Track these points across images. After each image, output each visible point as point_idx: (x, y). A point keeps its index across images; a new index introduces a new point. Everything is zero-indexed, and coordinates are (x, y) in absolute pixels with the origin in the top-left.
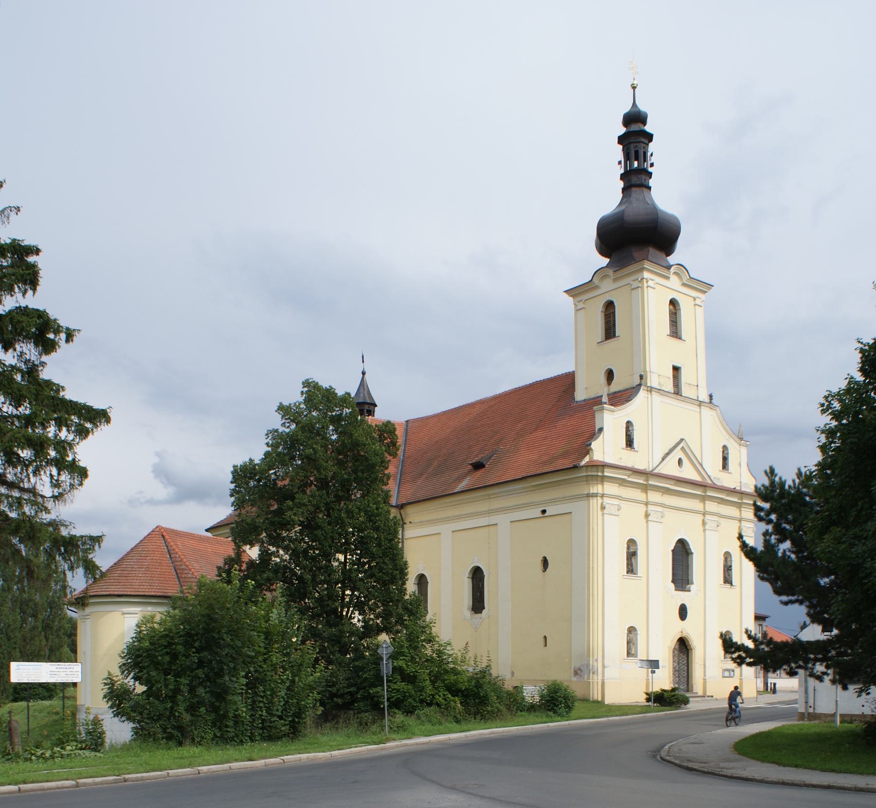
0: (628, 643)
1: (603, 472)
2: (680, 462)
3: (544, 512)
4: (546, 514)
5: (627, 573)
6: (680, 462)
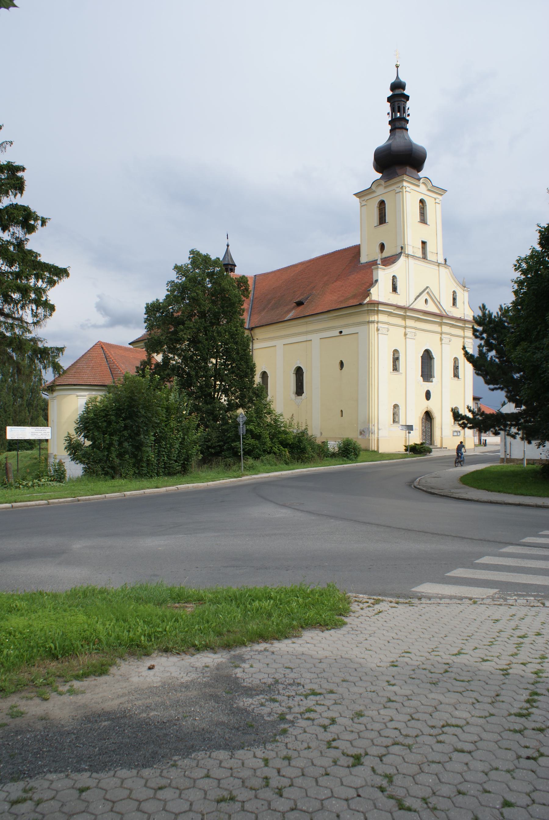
0: (394, 414)
1: (378, 307)
2: (426, 301)
3: (341, 332)
5: (393, 370)
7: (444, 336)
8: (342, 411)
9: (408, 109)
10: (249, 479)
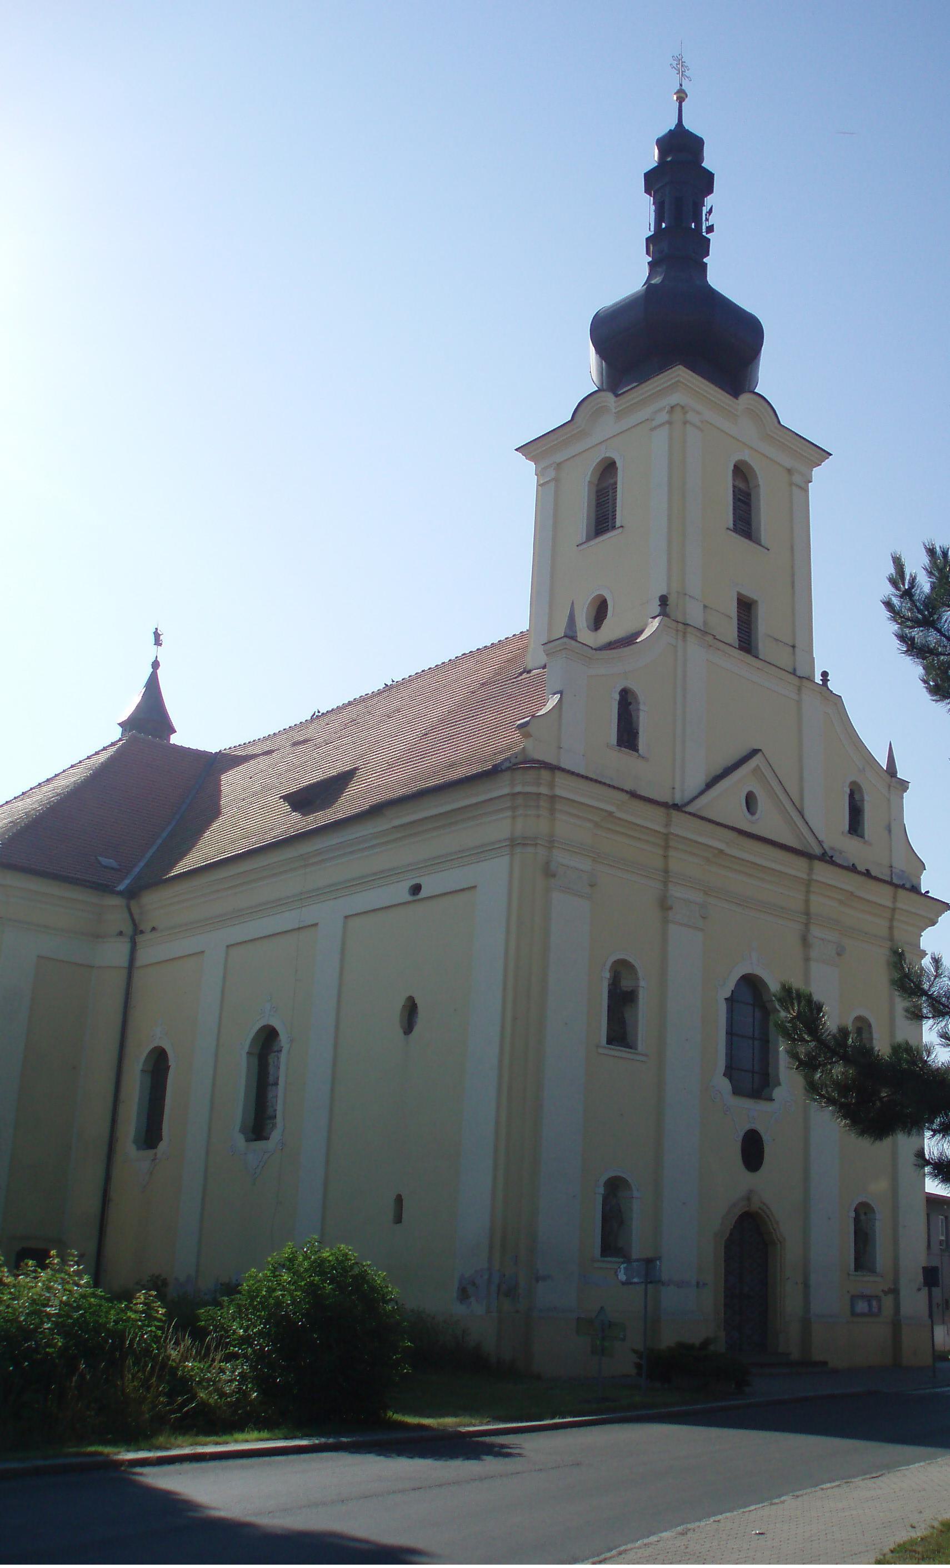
0: (605, 1219)
1: (552, 785)
2: (750, 801)
3: (416, 889)
4: (423, 894)
5: (610, 1041)
6: (750, 801)
7: (689, 629)
8: (399, 1200)
9: (710, 212)
10: (205, 1444)
